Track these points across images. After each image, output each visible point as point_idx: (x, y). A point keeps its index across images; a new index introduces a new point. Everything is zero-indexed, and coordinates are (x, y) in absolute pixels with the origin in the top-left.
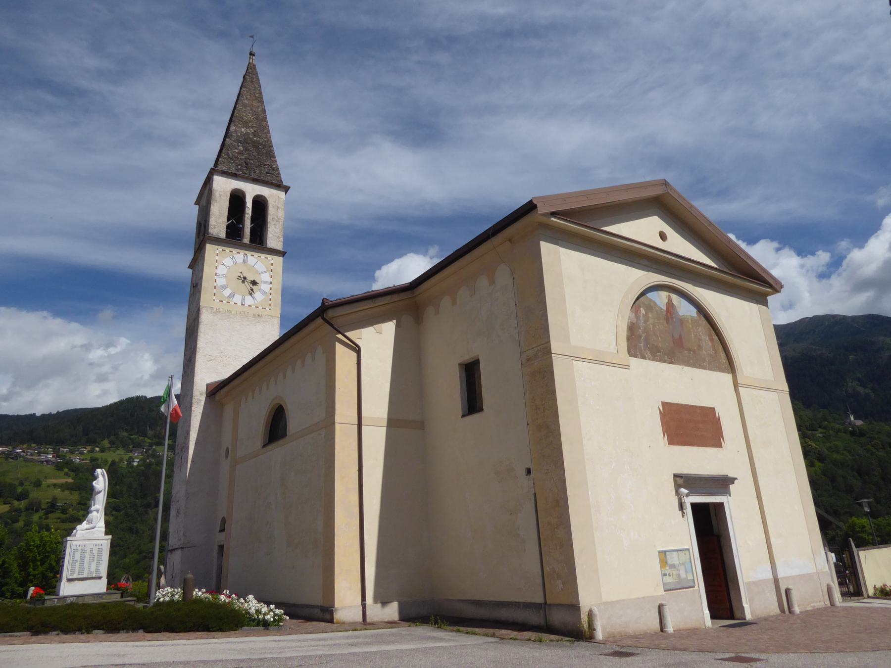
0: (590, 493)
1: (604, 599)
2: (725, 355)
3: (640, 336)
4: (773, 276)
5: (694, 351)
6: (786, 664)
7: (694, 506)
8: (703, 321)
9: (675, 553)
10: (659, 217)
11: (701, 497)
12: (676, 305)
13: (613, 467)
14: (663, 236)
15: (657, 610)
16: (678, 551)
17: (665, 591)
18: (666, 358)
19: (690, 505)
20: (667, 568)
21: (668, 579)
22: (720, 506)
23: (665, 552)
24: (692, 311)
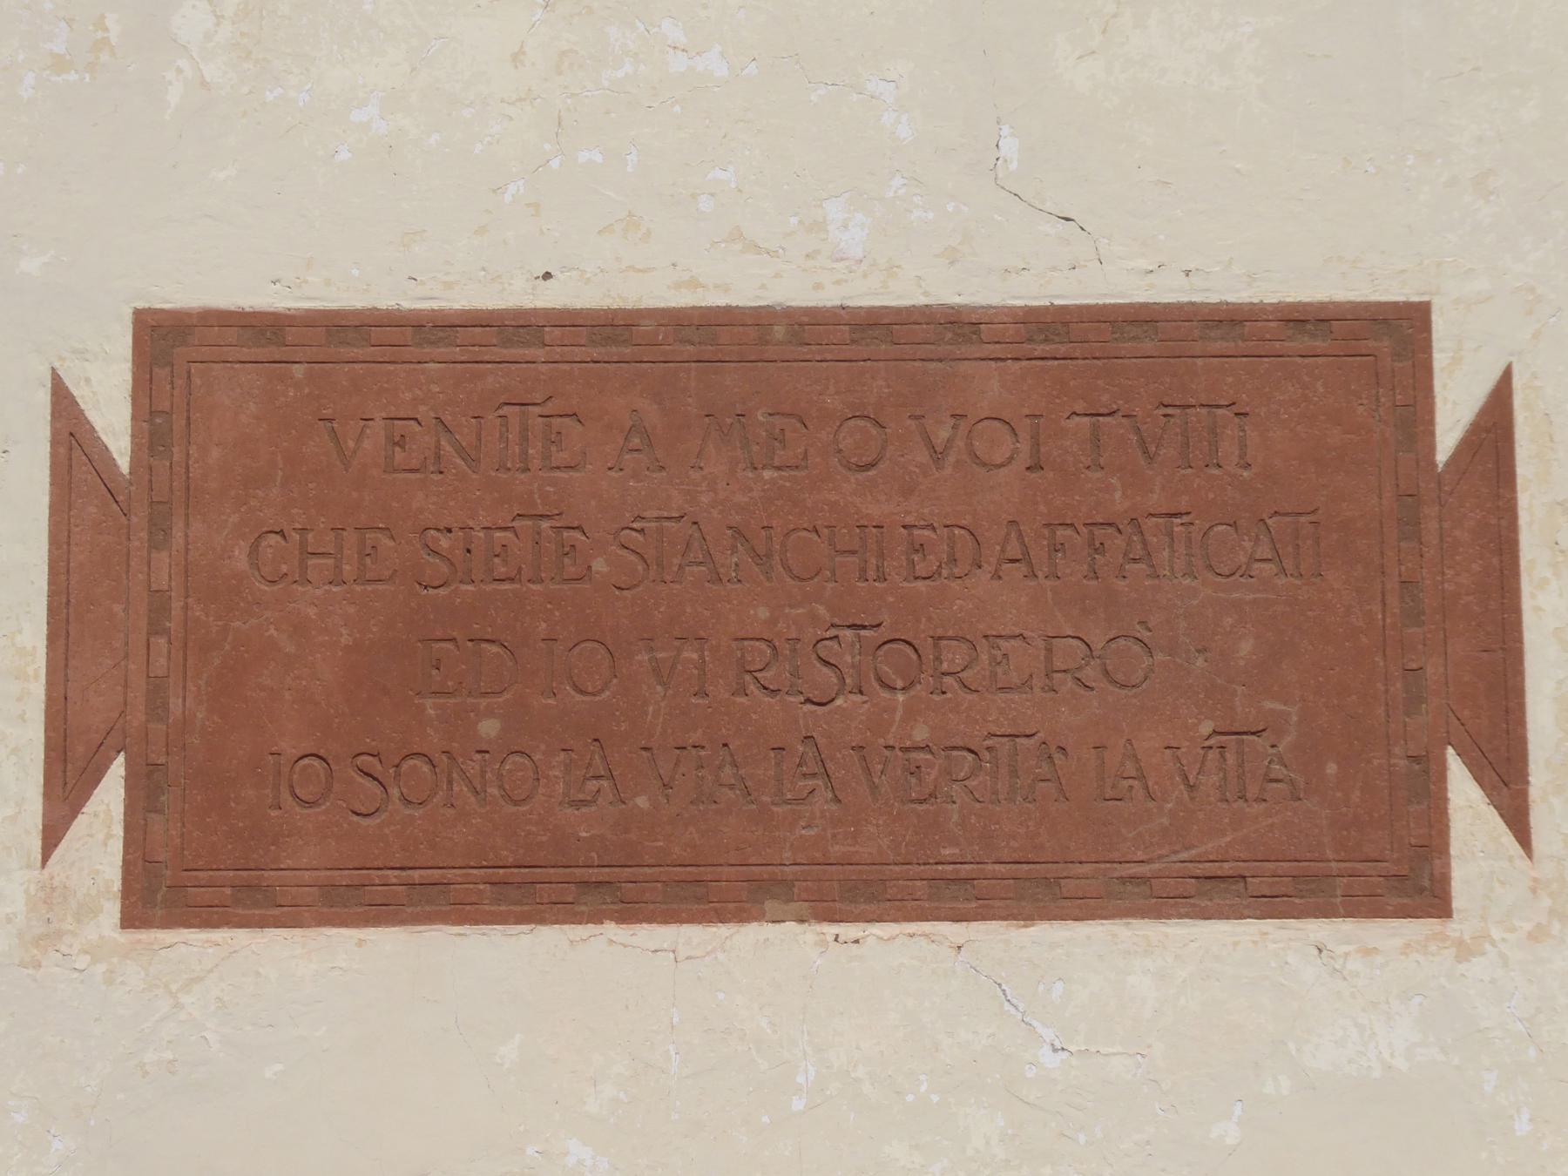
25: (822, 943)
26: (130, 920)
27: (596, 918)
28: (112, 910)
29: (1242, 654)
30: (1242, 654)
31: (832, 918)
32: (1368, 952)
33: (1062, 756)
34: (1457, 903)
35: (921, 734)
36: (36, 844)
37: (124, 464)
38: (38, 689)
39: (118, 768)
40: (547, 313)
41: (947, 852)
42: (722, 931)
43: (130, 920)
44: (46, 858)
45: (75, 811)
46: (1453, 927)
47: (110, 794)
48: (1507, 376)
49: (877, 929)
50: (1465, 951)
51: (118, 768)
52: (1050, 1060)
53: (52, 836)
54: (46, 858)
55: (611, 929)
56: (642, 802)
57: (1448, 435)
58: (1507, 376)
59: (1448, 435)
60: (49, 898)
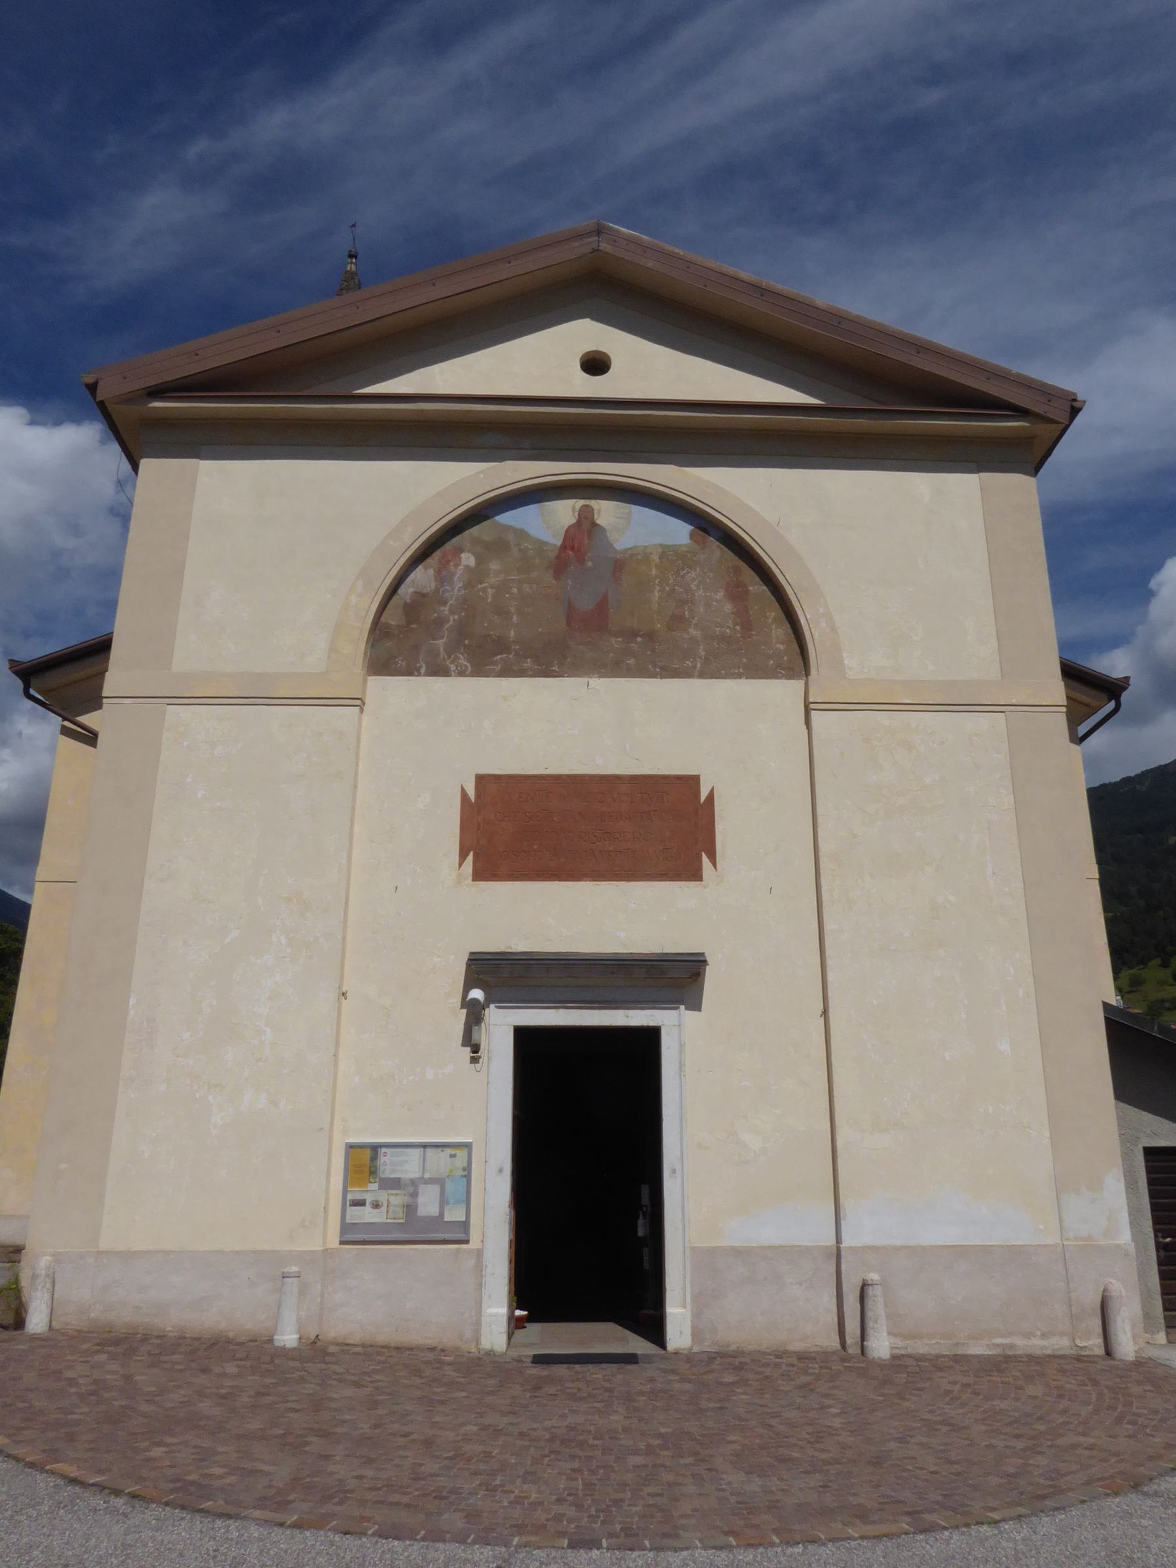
0: (132, 1001)
1: (104, 1245)
2: (790, 631)
3: (439, 623)
4: (526, 504)
5: (651, 636)
6: (394, 1479)
7: (524, 1036)
8: (716, 550)
9: (417, 1152)
10: (593, 319)
11: (561, 1011)
12: (604, 526)
13: (227, 940)
14: (595, 364)
15: (859, 1288)
16: (425, 1146)
17: (342, 1243)
18: (528, 664)
19: (652, 1024)
20: (374, 1186)
21: (367, 1215)
22: (650, 1037)
23: (375, 1148)
24: (679, 532)
25: (593, 885)
26: (474, 880)
27: (555, 880)
28: (471, 878)
29: (850, 1498)
30: (850, 1498)
31: (595, 881)
32: (688, 887)
33: (1036, 1518)
34: (702, 1009)
35: (611, 848)
36: (457, 866)
37: (473, 801)
38: (458, 840)
39: (472, 853)
40: (547, 775)
41: (616, 869)
42: (576, 883)
43: (474, 880)
44: (459, 868)
45: (463, 862)
46: (703, 883)
47: (470, 858)
48: (713, 787)
49: (603, 883)
50: (705, 887)
51: (472, 853)
52: (633, 906)
53: (460, 865)
54: (459, 868)
55: (557, 882)
56: (562, 860)
57: (703, 798)
58: (713, 787)
59: (703, 798)
60: (460, 875)
